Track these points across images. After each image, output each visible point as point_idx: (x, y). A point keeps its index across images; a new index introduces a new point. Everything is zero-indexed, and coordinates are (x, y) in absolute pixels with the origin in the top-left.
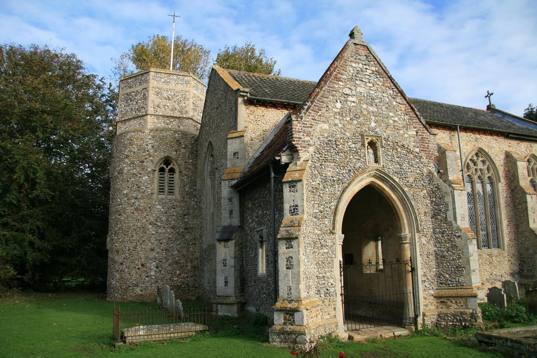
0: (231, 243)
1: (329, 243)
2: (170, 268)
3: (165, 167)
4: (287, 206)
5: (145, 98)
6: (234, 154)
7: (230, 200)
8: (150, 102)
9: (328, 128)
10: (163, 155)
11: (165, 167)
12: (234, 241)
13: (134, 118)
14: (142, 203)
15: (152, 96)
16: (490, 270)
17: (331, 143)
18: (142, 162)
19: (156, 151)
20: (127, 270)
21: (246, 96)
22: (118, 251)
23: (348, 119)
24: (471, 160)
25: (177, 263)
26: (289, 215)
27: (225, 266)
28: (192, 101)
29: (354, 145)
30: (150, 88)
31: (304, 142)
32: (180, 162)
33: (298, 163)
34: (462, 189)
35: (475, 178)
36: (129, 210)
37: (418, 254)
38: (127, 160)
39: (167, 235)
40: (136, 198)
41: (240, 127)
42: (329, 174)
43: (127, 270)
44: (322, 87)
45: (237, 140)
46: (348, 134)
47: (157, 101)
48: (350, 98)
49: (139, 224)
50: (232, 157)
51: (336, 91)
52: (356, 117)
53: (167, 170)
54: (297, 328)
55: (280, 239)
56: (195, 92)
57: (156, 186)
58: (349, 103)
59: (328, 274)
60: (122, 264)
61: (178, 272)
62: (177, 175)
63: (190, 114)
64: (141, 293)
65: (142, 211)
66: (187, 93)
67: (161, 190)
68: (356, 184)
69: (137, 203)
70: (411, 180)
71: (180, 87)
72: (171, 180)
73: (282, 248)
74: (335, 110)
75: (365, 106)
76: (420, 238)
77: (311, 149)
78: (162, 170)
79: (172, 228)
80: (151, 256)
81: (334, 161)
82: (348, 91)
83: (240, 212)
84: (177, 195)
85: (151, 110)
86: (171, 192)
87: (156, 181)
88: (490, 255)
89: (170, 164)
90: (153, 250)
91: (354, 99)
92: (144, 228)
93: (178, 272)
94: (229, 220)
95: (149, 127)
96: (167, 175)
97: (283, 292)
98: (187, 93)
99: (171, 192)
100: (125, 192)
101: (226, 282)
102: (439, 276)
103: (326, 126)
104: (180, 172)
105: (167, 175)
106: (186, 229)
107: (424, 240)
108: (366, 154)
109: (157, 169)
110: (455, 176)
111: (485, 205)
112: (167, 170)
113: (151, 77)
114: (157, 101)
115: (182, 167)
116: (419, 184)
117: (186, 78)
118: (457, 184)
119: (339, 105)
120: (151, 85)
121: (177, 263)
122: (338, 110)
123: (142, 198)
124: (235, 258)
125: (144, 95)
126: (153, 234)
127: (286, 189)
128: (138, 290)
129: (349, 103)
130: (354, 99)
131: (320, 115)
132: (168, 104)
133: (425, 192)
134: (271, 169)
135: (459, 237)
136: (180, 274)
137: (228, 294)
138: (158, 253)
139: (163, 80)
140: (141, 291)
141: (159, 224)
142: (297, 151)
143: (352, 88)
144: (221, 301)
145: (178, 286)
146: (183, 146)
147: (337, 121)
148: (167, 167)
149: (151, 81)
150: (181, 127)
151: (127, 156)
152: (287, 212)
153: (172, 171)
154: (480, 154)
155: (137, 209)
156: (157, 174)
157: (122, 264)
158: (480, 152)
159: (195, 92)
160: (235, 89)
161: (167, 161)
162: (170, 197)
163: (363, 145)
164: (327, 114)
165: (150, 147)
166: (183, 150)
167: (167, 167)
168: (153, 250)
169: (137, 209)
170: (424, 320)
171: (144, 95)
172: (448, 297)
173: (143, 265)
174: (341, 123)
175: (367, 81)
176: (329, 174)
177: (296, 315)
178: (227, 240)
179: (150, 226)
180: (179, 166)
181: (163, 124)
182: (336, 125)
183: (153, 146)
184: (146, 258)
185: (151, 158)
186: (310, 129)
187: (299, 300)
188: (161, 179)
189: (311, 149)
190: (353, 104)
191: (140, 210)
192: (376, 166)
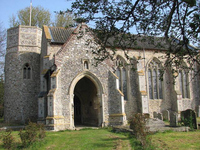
0: (43, 98)
1: (67, 97)
2: (29, 109)
3: (26, 67)
4: (52, 85)
5: (18, 38)
6: (46, 64)
7: (44, 82)
8: (19, 40)
9: (68, 57)
10: (25, 62)
11: (26, 67)
12: (44, 97)
13: (13, 47)
14: (16, 83)
15: (20, 38)
16: (157, 108)
17: (69, 64)
18: (17, 65)
19: (22, 61)
20: (11, 110)
21: (50, 41)
22: (7, 103)
23: (76, 53)
24: (150, 62)
25: (32, 107)
26: (52, 88)
27: (41, 106)
28: (38, 39)
29: (78, 63)
30: (20, 34)
31: (59, 63)
32: (33, 65)
33: (57, 70)
34: (142, 75)
35: (152, 70)
36: (12, 85)
37: (103, 101)
38: (10, 65)
39: (27, 95)
40: (14, 81)
41: (48, 54)
42: (68, 73)
43: (11, 110)
44: (67, 43)
45: (47, 59)
46: (76, 59)
47: (23, 39)
48: (78, 46)
49: (16, 91)
50: (45, 65)
51: (72, 44)
52: (80, 53)
53: (27, 68)
54: (52, 125)
55: (48, 96)
56: (39, 35)
57: (22, 76)
58: (77, 48)
59: (67, 108)
60: (9, 108)
61: (32, 111)
62: (31, 70)
63: (37, 44)
64: (17, 119)
65: (17, 86)
66: (35, 36)
67: (25, 77)
68: (79, 77)
69: (15, 83)
70: (101, 74)
71: (32, 33)
72: (29, 73)
73: (49, 99)
74: (71, 51)
75: (84, 48)
76: (104, 95)
77: (62, 65)
78: (25, 69)
79: (29, 93)
80: (21, 104)
81: (70, 69)
82: (77, 43)
83: (47, 86)
84: (31, 79)
85: (20, 44)
86: (29, 78)
87: (22, 73)
88: (158, 102)
89: (28, 66)
90: (21, 102)
91: (79, 46)
92: (18, 94)
93: (32, 111)
94: (43, 90)
95: (19, 51)
96: (27, 70)
97: (49, 114)
98: (35, 36)
99: (29, 78)
100: (10, 78)
101: (42, 112)
102: (111, 109)
103: (68, 57)
104: (33, 69)
105: (27, 70)
106: (35, 93)
107: (106, 96)
108: (83, 66)
109: (23, 68)
110: (140, 70)
111: (151, 81)
112: (27, 68)
113: (20, 29)
114: (23, 39)
115: (34, 67)
116: (105, 76)
117: (35, 29)
118: (141, 73)
119: (73, 49)
120: (20, 32)
121: (32, 107)
122: (73, 51)
123: (17, 80)
124: (45, 103)
125: (17, 37)
126: (22, 95)
127: (51, 79)
128: (16, 119)
129: (77, 48)
130: (79, 46)
131: (65, 53)
132: (27, 41)
133: (107, 78)
134: (49, 73)
135: (118, 95)
136: (33, 111)
137: (42, 117)
138: (23, 103)
139: (25, 30)
140: (17, 119)
141: (24, 91)
142: (56, 66)
143: (79, 42)
144: (40, 119)
145: (32, 116)
146: (34, 58)
147: (72, 55)
148: (27, 67)
149: (20, 31)
150: (33, 50)
151: (11, 63)
152: (51, 87)
153: (29, 69)
154: (155, 60)
155: (15, 85)
156: (23, 70)
157: (9, 108)
158: (154, 59)
159: (39, 35)
160: (47, 38)
161: (27, 65)
162: (28, 80)
163: (82, 63)
164: (68, 53)
165: (20, 59)
166: (34, 60)
167: (27, 67)
168: (21, 102)
169: (15, 85)
170: (104, 125)
171: (17, 37)
172: (114, 116)
173: (17, 108)
174: (74, 55)
175: (85, 39)
176: (68, 73)
177: (52, 121)
178: (42, 97)
179: (20, 92)
180: (32, 67)
181: (25, 49)
182: (72, 56)
183: (21, 59)
184: (19, 105)
185: (20, 64)
186: (61, 58)
187: (53, 116)
188: (25, 72)
189: (62, 65)
190: (79, 48)
191: (16, 85)
192: (87, 70)
